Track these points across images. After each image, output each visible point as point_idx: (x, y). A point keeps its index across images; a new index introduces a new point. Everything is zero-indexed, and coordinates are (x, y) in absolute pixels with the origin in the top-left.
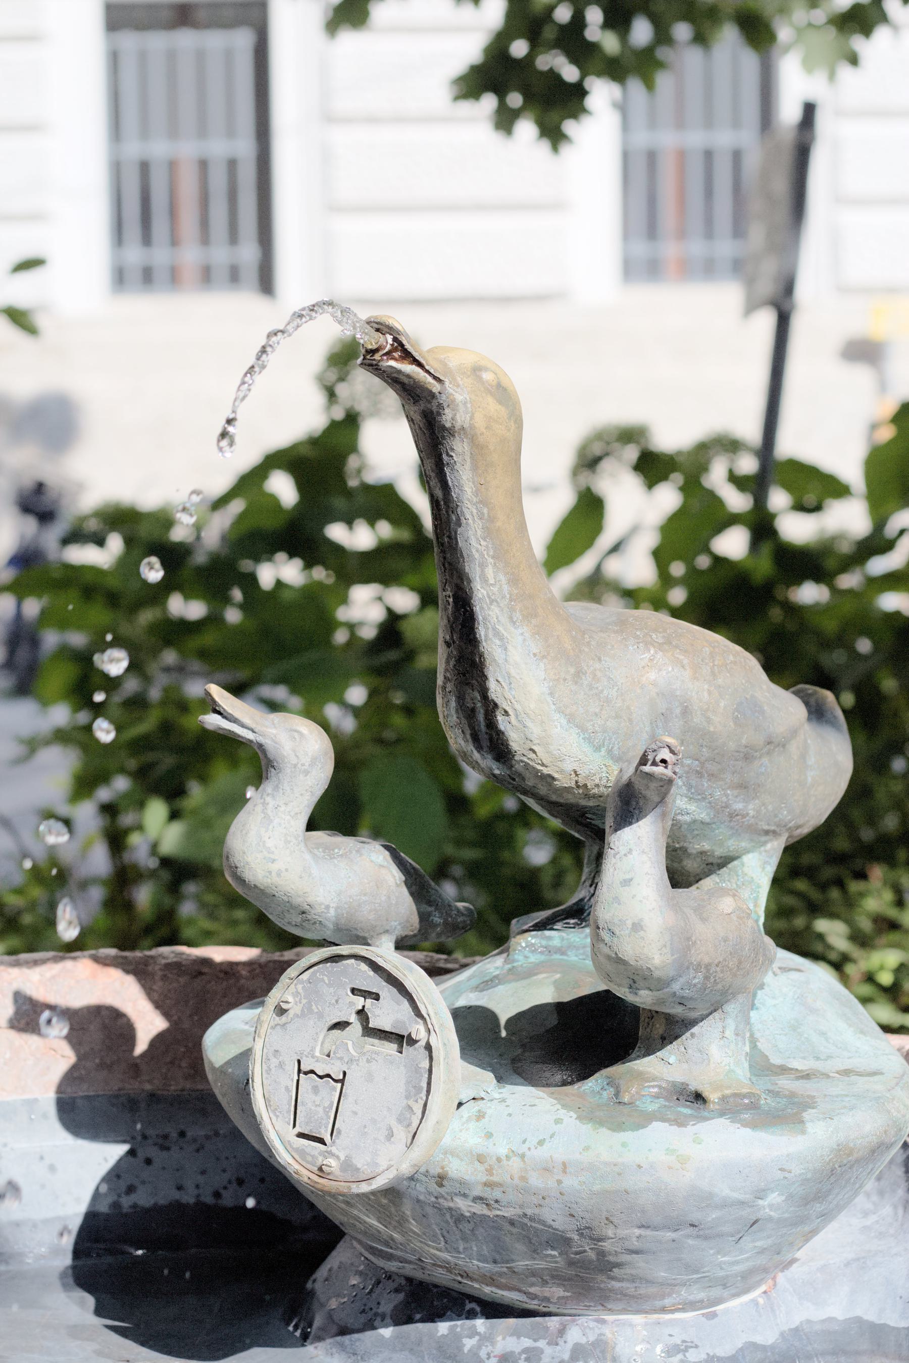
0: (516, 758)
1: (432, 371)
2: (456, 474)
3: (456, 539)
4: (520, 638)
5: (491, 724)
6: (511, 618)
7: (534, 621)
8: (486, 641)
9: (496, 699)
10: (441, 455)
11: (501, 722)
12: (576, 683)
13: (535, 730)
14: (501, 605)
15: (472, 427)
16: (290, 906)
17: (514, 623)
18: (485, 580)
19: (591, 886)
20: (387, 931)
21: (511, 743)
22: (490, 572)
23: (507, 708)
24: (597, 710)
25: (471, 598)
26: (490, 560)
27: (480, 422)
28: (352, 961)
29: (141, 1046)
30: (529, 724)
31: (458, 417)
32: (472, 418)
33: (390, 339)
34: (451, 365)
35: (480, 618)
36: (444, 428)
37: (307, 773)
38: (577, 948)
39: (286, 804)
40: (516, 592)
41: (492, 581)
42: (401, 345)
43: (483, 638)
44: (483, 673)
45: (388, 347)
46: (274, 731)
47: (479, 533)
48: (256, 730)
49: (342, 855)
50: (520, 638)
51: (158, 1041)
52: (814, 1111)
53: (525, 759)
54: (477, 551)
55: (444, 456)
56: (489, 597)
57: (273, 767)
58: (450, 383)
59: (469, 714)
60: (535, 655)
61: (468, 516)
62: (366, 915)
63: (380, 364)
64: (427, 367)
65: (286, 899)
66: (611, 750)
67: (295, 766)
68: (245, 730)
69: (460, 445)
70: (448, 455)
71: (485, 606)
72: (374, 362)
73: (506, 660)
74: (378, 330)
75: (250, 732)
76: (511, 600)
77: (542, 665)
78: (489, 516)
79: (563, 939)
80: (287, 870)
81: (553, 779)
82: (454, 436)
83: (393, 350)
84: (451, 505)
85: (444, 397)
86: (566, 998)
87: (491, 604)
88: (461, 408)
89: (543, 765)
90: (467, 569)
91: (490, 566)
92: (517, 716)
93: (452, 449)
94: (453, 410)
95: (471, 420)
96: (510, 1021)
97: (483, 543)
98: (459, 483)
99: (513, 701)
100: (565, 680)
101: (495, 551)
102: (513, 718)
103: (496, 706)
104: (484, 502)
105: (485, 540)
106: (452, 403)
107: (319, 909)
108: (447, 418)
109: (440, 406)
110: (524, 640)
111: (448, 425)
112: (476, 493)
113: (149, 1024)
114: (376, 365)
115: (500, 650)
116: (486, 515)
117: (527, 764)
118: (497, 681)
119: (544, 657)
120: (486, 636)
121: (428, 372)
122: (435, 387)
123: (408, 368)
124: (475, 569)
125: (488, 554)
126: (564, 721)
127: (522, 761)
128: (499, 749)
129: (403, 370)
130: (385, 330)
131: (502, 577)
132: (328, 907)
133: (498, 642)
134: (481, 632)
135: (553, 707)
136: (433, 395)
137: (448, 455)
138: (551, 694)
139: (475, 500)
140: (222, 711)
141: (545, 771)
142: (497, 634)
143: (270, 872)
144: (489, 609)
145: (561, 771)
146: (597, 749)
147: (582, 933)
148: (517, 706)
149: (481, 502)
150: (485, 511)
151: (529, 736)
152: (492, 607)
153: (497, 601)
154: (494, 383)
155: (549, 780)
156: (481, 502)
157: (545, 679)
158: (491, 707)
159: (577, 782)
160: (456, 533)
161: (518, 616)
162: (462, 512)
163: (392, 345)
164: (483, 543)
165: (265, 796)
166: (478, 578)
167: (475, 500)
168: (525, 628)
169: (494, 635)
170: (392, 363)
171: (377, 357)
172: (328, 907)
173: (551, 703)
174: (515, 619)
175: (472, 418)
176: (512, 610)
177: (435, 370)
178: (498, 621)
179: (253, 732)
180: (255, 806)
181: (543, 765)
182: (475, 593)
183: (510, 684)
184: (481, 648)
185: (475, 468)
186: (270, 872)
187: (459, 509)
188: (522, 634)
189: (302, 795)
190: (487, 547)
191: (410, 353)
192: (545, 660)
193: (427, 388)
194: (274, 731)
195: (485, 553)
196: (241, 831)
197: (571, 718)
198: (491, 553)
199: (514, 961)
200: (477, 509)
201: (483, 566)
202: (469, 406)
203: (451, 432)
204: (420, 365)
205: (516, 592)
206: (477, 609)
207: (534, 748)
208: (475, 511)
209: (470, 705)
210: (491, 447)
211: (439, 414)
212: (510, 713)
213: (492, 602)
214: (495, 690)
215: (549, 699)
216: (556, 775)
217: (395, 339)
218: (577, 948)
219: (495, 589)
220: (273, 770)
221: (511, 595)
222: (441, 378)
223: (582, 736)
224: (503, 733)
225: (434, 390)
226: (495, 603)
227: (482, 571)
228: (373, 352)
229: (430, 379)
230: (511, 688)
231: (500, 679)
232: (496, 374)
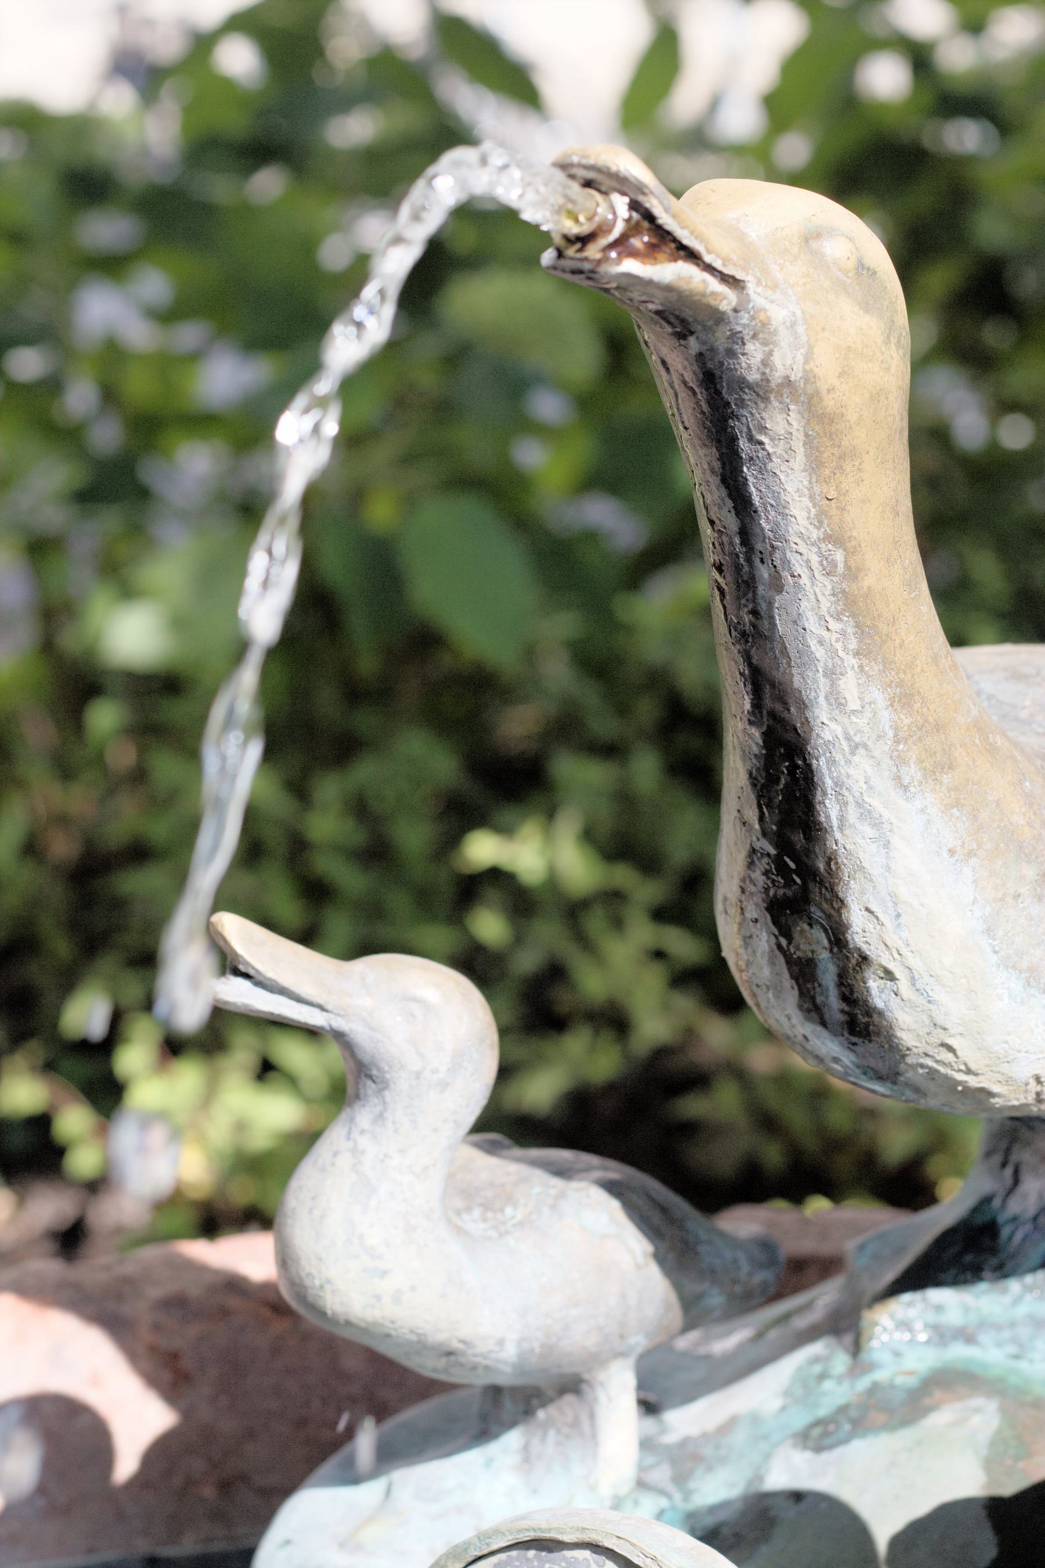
0: (910, 1060)
1: (718, 264)
2: (770, 480)
3: (772, 618)
5: (852, 998)
6: (898, 778)
7: (946, 779)
8: (841, 828)
9: (865, 947)
10: (734, 439)
11: (877, 992)
13: (952, 1009)
14: (876, 753)
15: (809, 377)
16: (422, 1346)
17: (906, 788)
18: (838, 702)
19: (1004, 1165)
20: (623, 1355)
21: (899, 1034)
22: (849, 686)
23: (891, 966)
25: (806, 741)
26: (851, 661)
27: (826, 367)
28: (586, 1554)
29: (126, 1465)
30: (939, 994)
31: (777, 360)
32: (808, 358)
33: (621, 203)
34: (753, 235)
35: (829, 782)
36: (742, 384)
37: (444, 1086)
38: (998, 1327)
39: (402, 1151)
41: (854, 704)
42: (649, 217)
43: (835, 823)
44: (832, 890)
45: (619, 228)
46: (366, 1002)
47: (825, 604)
48: (329, 1007)
49: (521, 1224)
51: (161, 1453)
52: (660, 330)
53: (930, 1062)
54: (821, 642)
55: (743, 444)
56: (848, 738)
57: (370, 1077)
58: (759, 282)
59: (803, 972)
60: (952, 852)
61: (798, 570)
62: (579, 1338)
63: (603, 269)
64: (708, 258)
65: (414, 1338)
67: (418, 1075)
68: (305, 1009)
69: (780, 418)
70: (751, 439)
71: (838, 757)
72: (587, 266)
73: (888, 868)
74: (588, 184)
75: (316, 1011)
78: (847, 567)
79: (967, 1309)
80: (413, 1288)
81: (991, 1094)
82: (766, 400)
83: (633, 229)
84: (759, 546)
85: (744, 318)
86: (1008, 1488)
87: (853, 753)
88: (784, 338)
89: (969, 1071)
90: (797, 681)
91: (850, 674)
92: (913, 981)
93: (763, 429)
94: (765, 344)
95: (806, 362)
96: (897, 1542)
97: (833, 625)
98: (777, 499)
99: (904, 950)
101: (861, 641)
102: (903, 985)
103: (864, 959)
104: (836, 539)
105: (839, 619)
106: (763, 332)
107: (481, 1348)
108: (751, 361)
109: (736, 337)
111: (753, 377)
112: (820, 519)
113: (137, 1419)
114: (593, 271)
115: (873, 847)
116: (841, 566)
117: (932, 1073)
118: (867, 909)
119: (971, 854)
120: (842, 819)
121: (709, 268)
122: (726, 298)
123: (669, 271)
124: (815, 681)
125: (845, 649)
127: (922, 1066)
128: (860, 1024)
129: (656, 278)
130: (606, 183)
131: (878, 696)
132: (501, 1342)
133: (870, 832)
134: (829, 810)
135: (994, 958)
136: (719, 318)
137: (751, 439)
138: (989, 931)
139: (815, 534)
140: (252, 972)
141: (973, 1082)
142: (867, 813)
143: (378, 1298)
144: (848, 762)
145: (1008, 1081)
147: (1005, 1291)
148: (913, 961)
149: (827, 538)
150: (839, 556)
151: (940, 1020)
152: (856, 759)
153: (865, 746)
154: (852, 264)
155: (983, 1096)
156: (827, 538)
158: (852, 964)
159: (1038, 1094)
160: (770, 604)
161: (912, 772)
162: (786, 562)
163: (628, 221)
164: (833, 625)
165: (355, 1134)
166: (822, 700)
167: (815, 534)
169: (861, 817)
170: (631, 266)
171: (593, 251)
172: (501, 1342)
175: (808, 358)
176: (900, 760)
177: (725, 261)
178: (871, 788)
179: (322, 1008)
180: (336, 1154)
181: (969, 1071)
182: (817, 730)
183: (898, 916)
184: (830, 844)
185: (815, 465)
186: (378, 1298)
187: (777, 555)
188: (923, 811)
189: (435, 1130)
190: (843, 633)
191: (668, 233)
192: (974, 861)
193: (709, 307)
194: (366, 1002)
195: (839, 646)
196: (310, 1211)
198: (853, 645)
199: (871, 1367)
200: (820, 553)
201: (832, 674)
203: (761, 391)
204: (691, 255)
206: (821, 765)
207: (950, 1041)
208: (815, 559)
209: (984, 1338)
210: (852, 416)
211: (731, 353)
212: (897, 975)
213: (855, 748)
214: (860, 929)
216: (995, 1089)
217: (634, 205)
218: (998, 1327)
219: (861, 721)
220: (369, 1083)
221: (896, 729)
222: (739, 275)
224: (881, 1014)
225: (725, 306)
226: (861, 751)
227: (833, 684)
228: (584, 240)
229: (714, 285)
230: (899, 925)
231: (873, 908)
232: (851, 239)
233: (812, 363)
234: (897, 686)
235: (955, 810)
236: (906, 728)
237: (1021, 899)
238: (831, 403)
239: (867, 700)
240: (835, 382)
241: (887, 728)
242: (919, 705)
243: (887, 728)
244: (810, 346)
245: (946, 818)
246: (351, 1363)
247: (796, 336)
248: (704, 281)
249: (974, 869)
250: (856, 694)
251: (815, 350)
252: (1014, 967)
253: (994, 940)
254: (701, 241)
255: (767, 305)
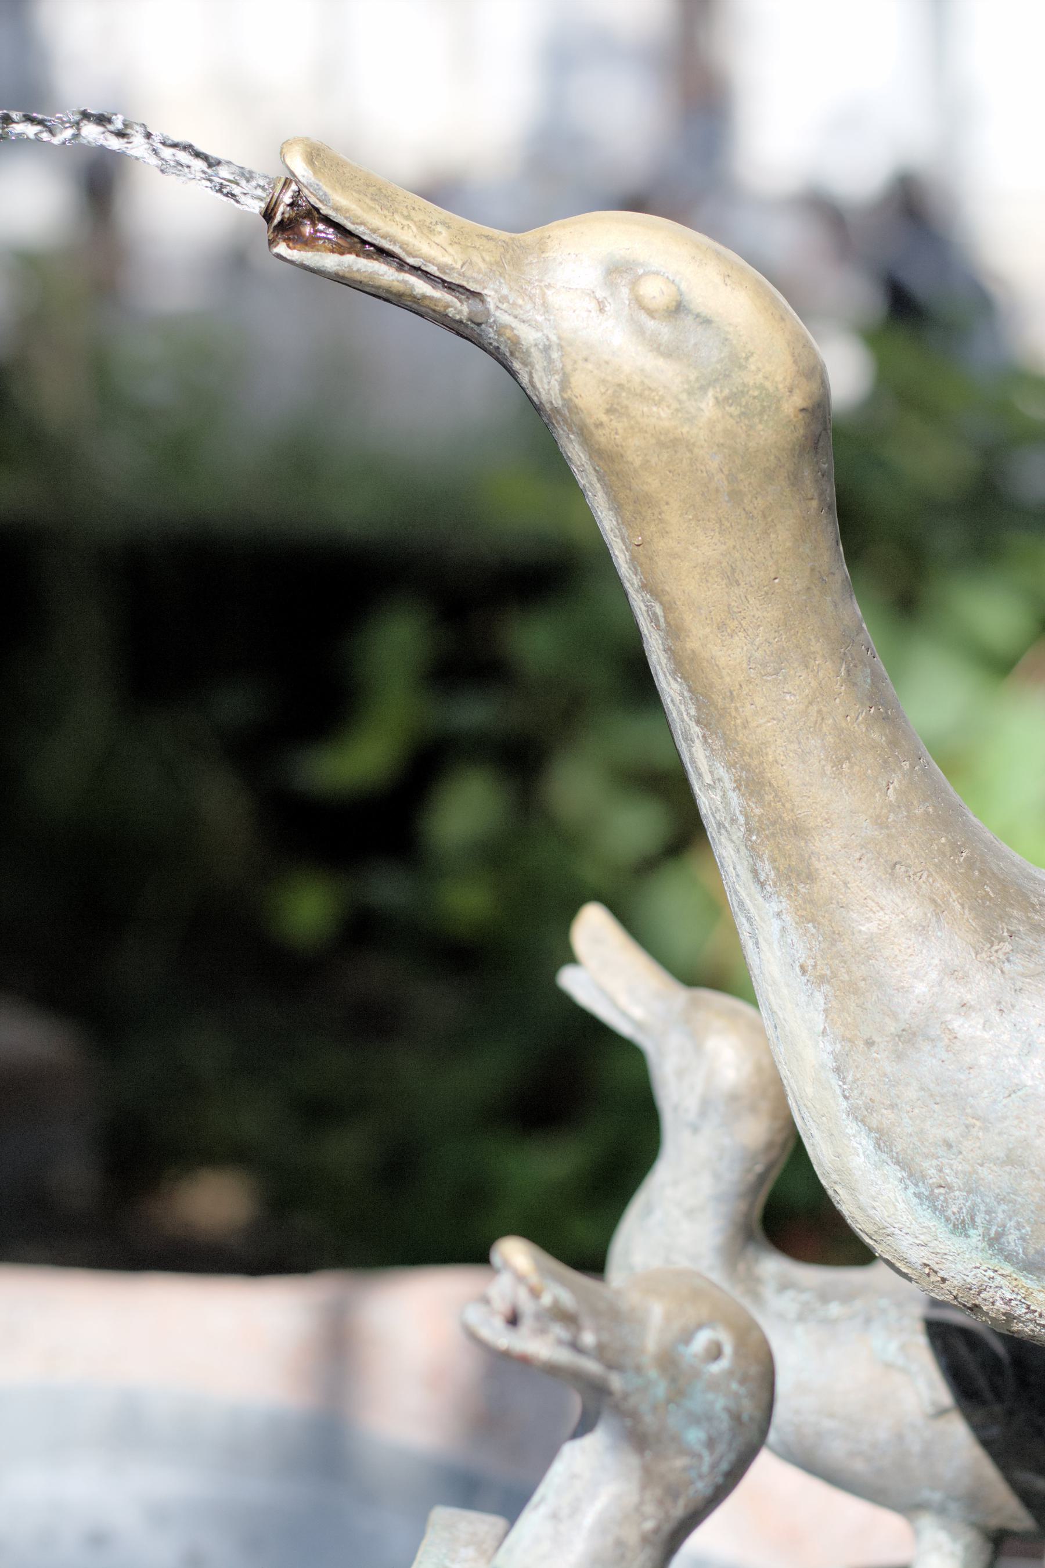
1: (432, 269)
4: (776, 925)
6: (755, 872)
12: (899, 1057)
14: (734, 838)
17: (762, 885)
24: (951, 1135)
40: (758, 811)
50: (776, 925)
60: (803, 970)
64: (411, 261)
66: (999, 1236)
76: (750, 831)
77: (819, 998)
100: (870, 1043)
110: (783, 929)
119: (822, 980)
126: (868, 1144)
131: (721, 771)
135: (844, 1104)
138: (837, 1070)
146: (960, 1227)
157: (824, 1032)
168: (785, 904)
173: (839, 1092)
174: (762, 878)
177: (441, 268)
188: (779, 914)
192: (825, 988)
197: (882, 1140)
202: (555, 355)
204: (382, 253)
205: (758, 811)
215: (835, 1082)
223: (912, 1189)
233: (569, 392)
234: (742, 769)
235: (810, 925)
236: (757, 819)
237: (874, 1048)
238: (603, 439)
239: (716, 777)
240: (604, 418)
241: (738, 813)
242: (771, 797)
243: (738, 813)
244: (564, 374)
245: (801, 931)
246: (999, 1348)
247: (550, 361)
248: (405, 282)
249: (826, 997)
250: (707, 767)
251: (572, 380)
252: (862, 1121)
253: (844, 1083)
254: (395, 243)
255: (514, 323)
